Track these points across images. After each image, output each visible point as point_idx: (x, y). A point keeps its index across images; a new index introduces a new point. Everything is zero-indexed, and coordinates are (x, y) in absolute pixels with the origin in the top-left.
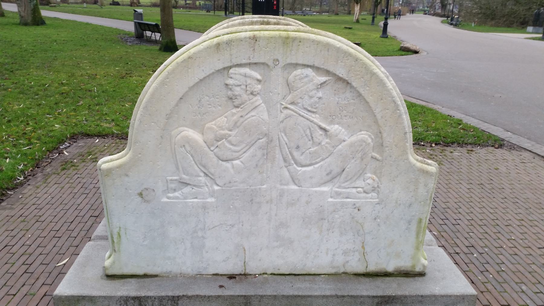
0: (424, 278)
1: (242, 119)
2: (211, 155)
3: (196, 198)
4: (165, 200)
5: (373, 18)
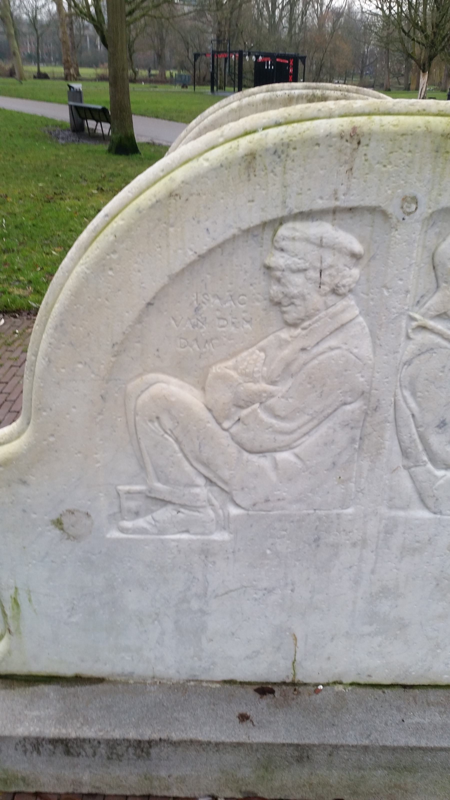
1: (304, 357)
2: (224, 439)
3: (187, 531)
4: (115, 534)
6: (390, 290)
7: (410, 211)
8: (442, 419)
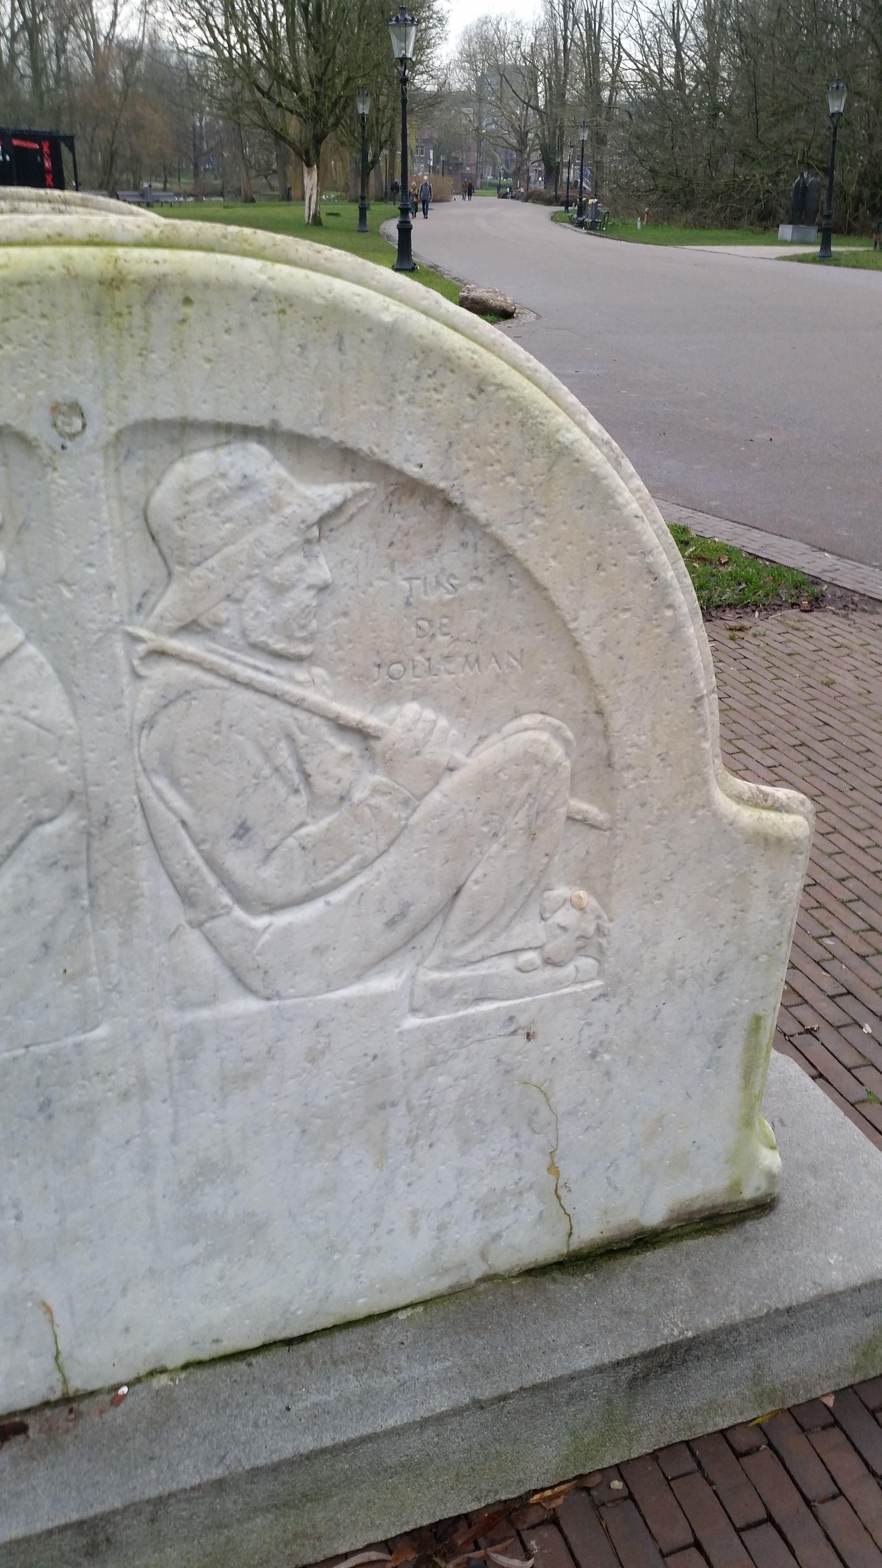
0: (773, 1218)
5: (363, 211)
6: (74, 588)
7: (73, 431)
8: (238, 821)
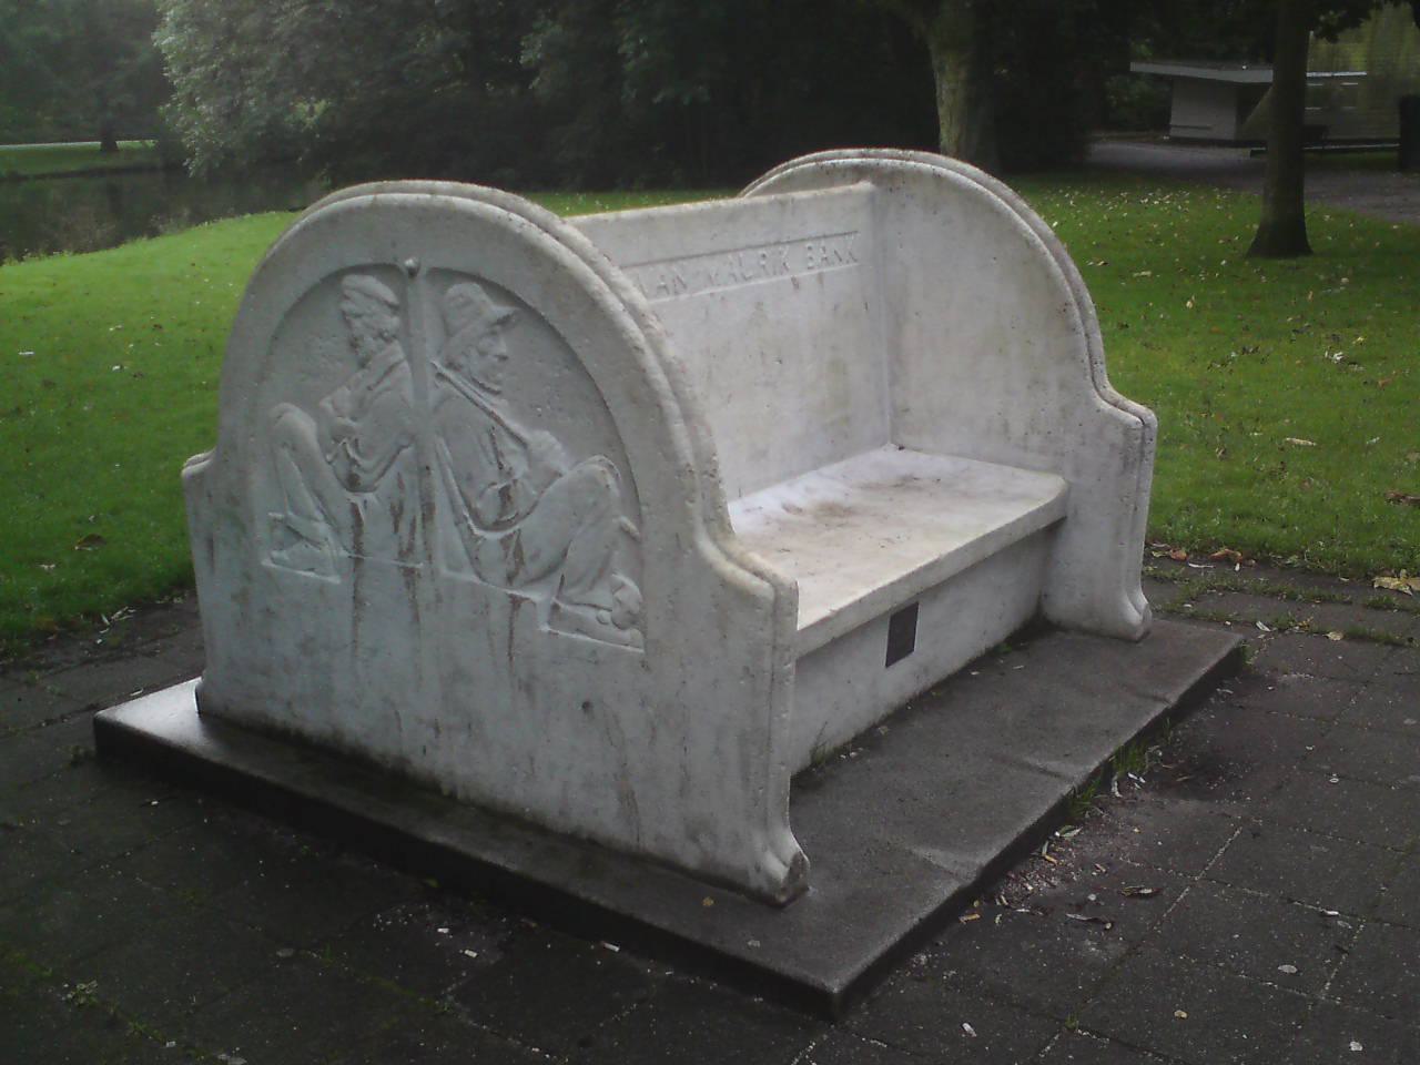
3: (312, 570)
